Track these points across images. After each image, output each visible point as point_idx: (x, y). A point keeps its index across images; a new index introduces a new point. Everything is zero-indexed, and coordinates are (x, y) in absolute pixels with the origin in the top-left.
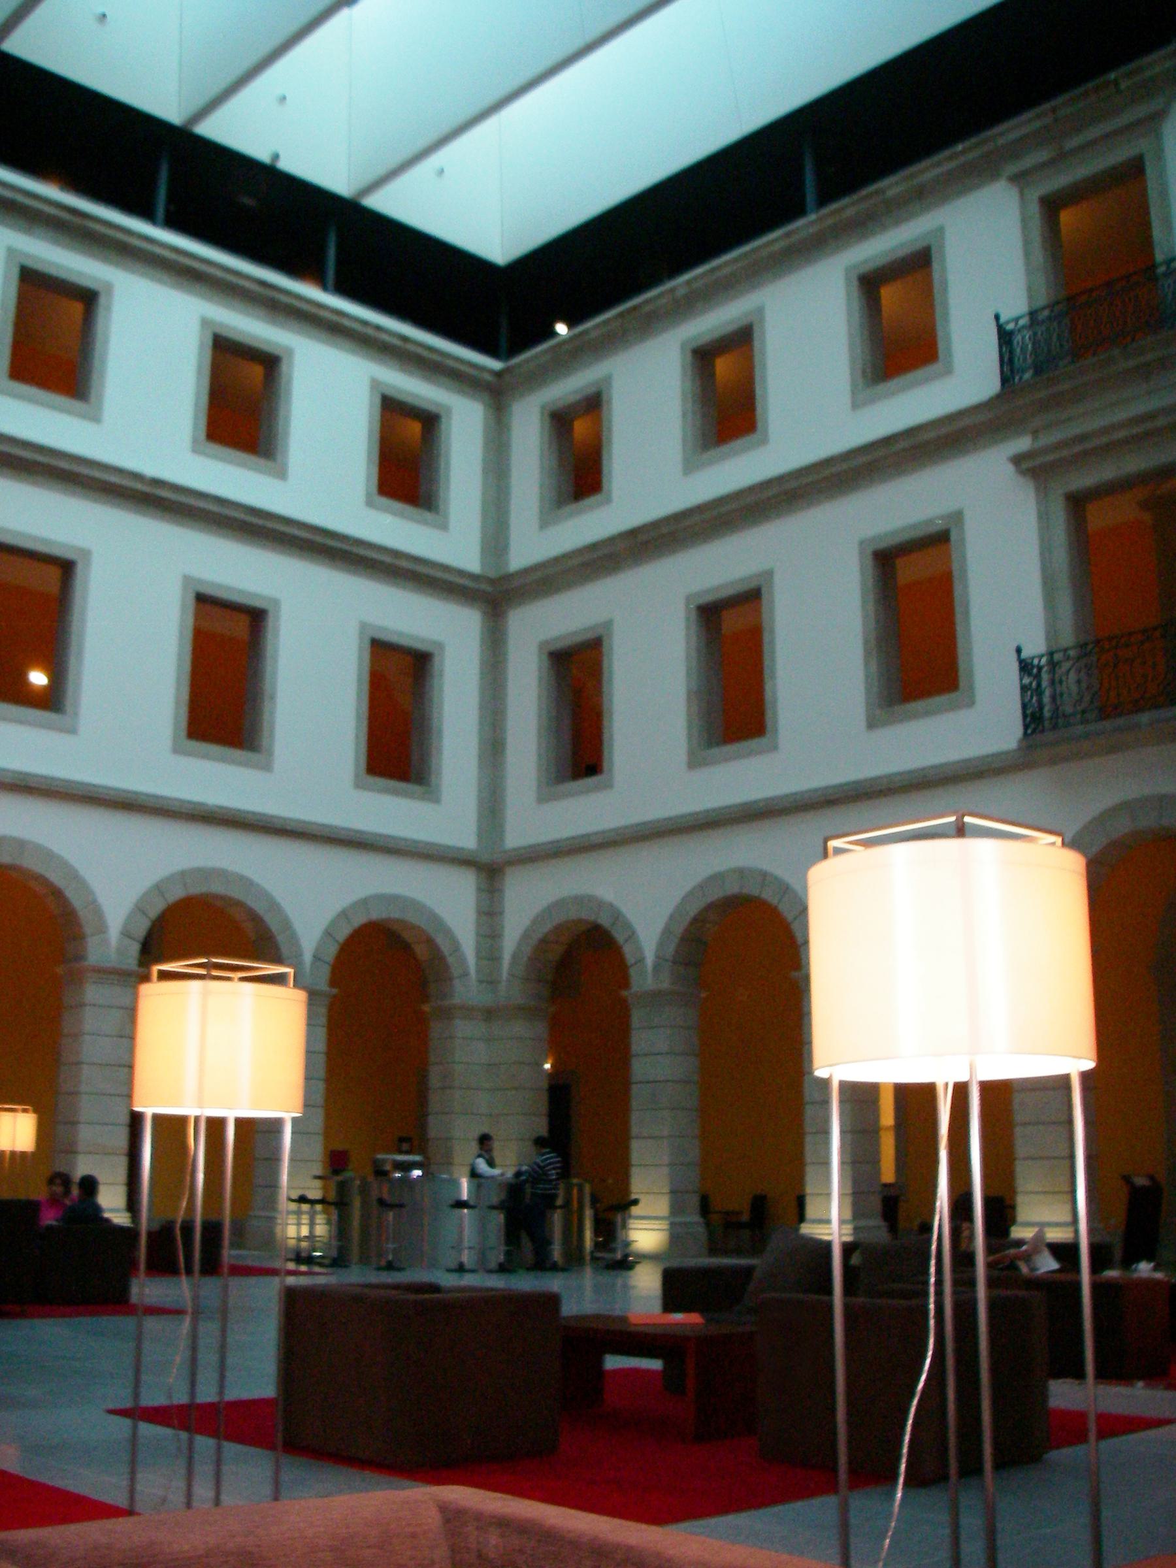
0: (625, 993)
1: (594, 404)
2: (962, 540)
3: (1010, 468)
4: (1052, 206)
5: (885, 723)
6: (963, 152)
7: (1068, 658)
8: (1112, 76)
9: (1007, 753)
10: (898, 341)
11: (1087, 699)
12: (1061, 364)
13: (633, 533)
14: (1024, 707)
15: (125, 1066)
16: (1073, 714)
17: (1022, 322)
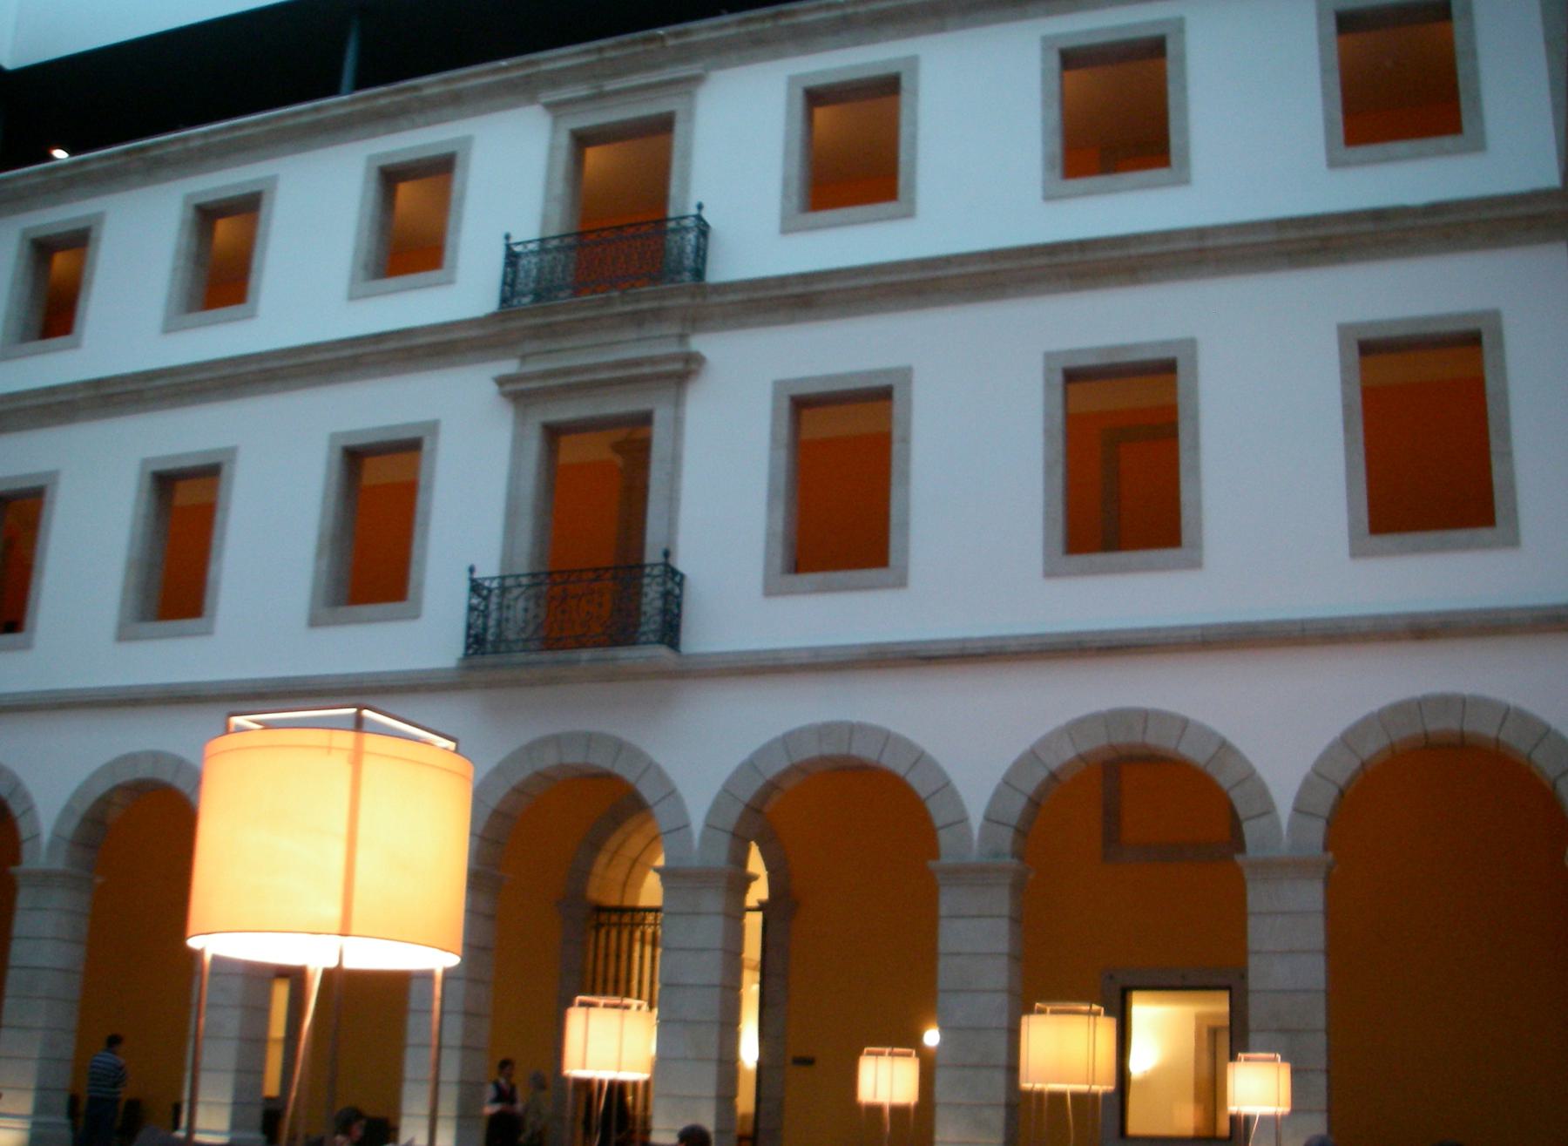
0: (932, 864)
1: (79, 241)
2: (434, 450)
3: (493, 388)
4: (582, 140)
5: (327, 624)
6: (506, 69)
7: (520, 585)
8: (661, 32)
9: (446, 670)
10: (407, 239)
11: (531, 628)
12: (562, 295)
13: (98, 383)
14: (469, 627)
16: (516, 641)
17: (532, 247)
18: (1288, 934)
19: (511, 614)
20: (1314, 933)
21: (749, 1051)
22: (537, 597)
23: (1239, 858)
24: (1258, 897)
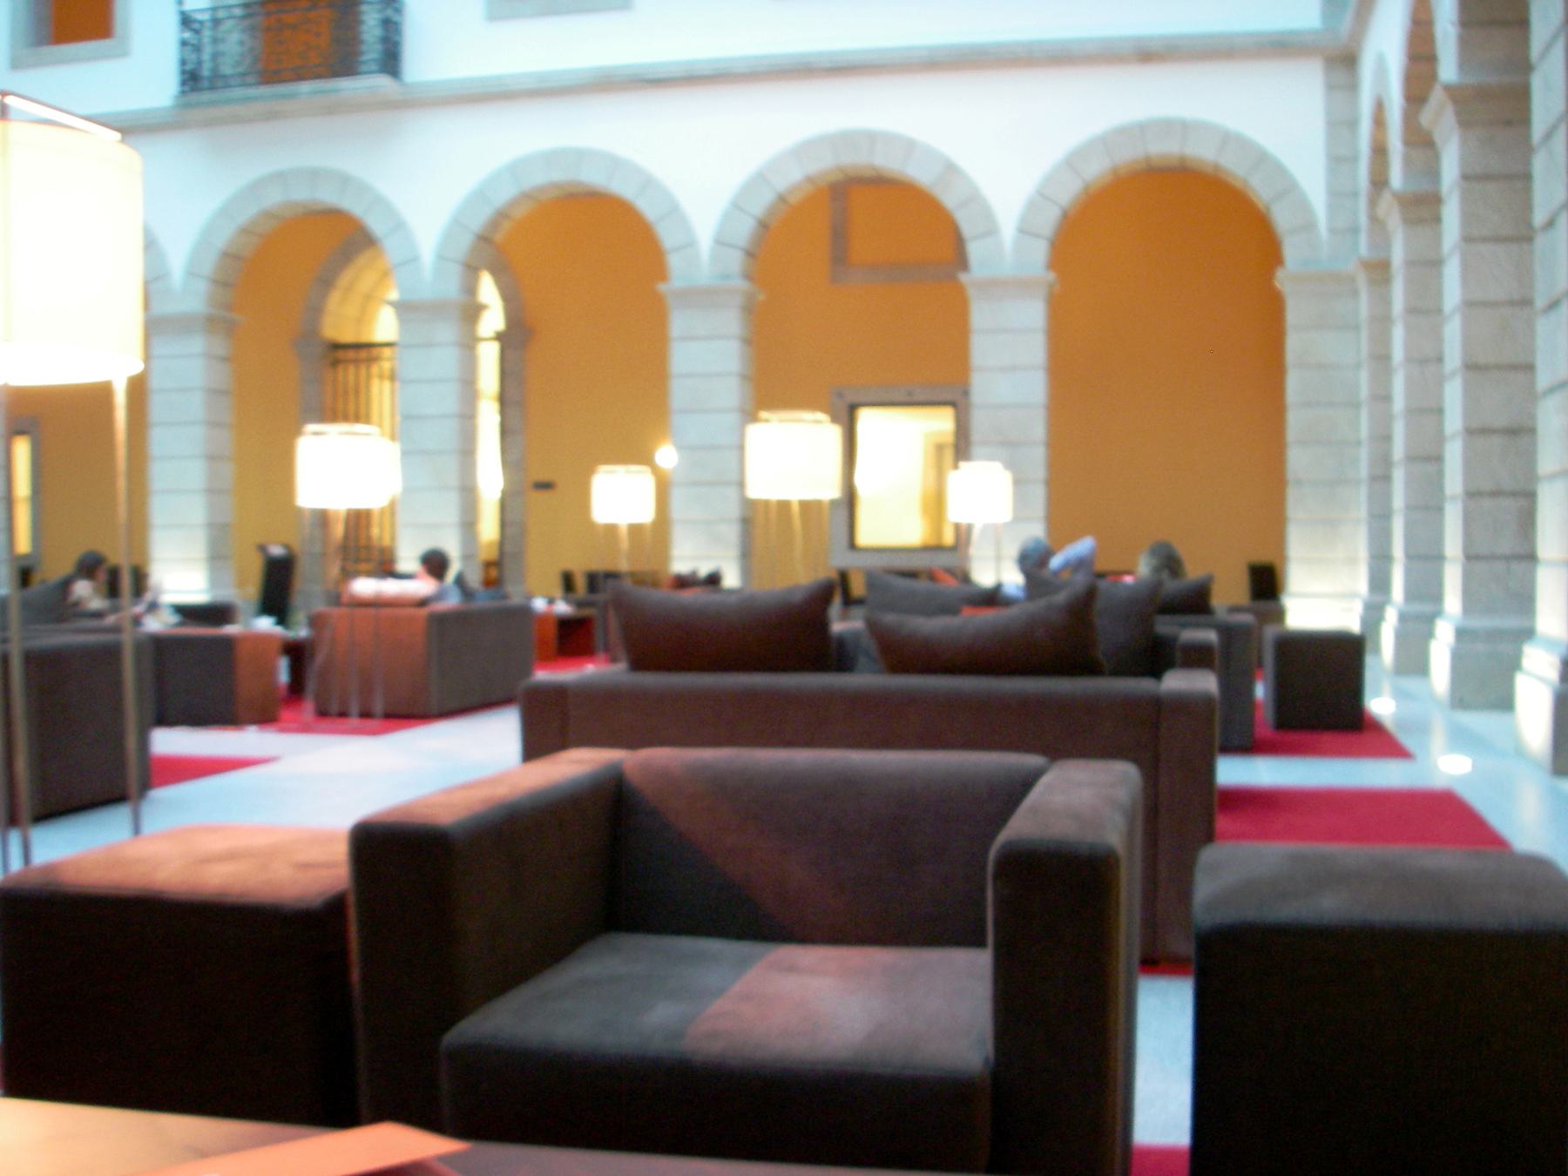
14: (183, 62)
15: (1514, 494)
18: (1010, 351)
19: (221, 47)
20: (1034, 350)
21: (491, 480)
22: (252, 28)
23: (964, 278)
24: (981, 315)
